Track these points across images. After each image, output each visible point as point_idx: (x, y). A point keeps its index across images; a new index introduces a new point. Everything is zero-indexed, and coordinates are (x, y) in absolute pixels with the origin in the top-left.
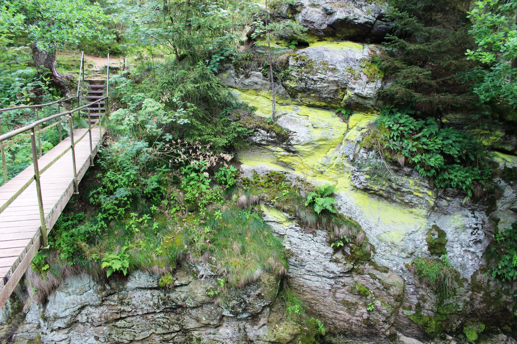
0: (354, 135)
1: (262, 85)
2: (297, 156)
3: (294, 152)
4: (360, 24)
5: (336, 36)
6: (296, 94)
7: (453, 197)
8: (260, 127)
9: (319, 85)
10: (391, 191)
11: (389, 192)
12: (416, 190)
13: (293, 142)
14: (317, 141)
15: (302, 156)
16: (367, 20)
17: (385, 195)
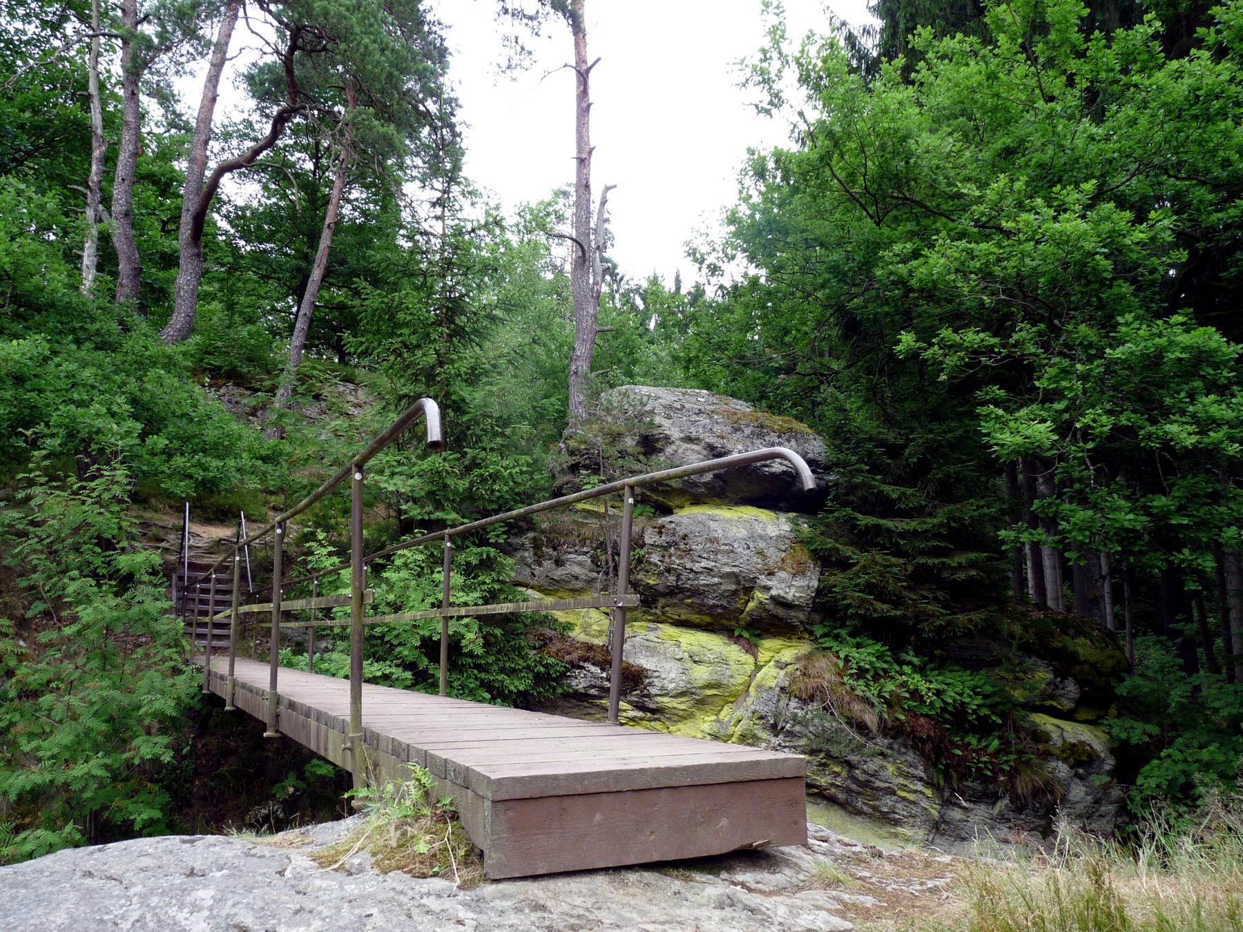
0: (771, 676)
1: (587, 581)
2: (659, 720)
3: (653, 711)
4: (773, 475)
5: (726, 497)
6: (655, 601)
7: (974, 802)
8: (586, 660)
9: (704, 580)
10: (854, 787)
11: (848, 791)
12: (904, 787)
13: (653, 691)
14: (701, 688)
15: (669, 719)
16: (785, 469)
17: (841, 796)
